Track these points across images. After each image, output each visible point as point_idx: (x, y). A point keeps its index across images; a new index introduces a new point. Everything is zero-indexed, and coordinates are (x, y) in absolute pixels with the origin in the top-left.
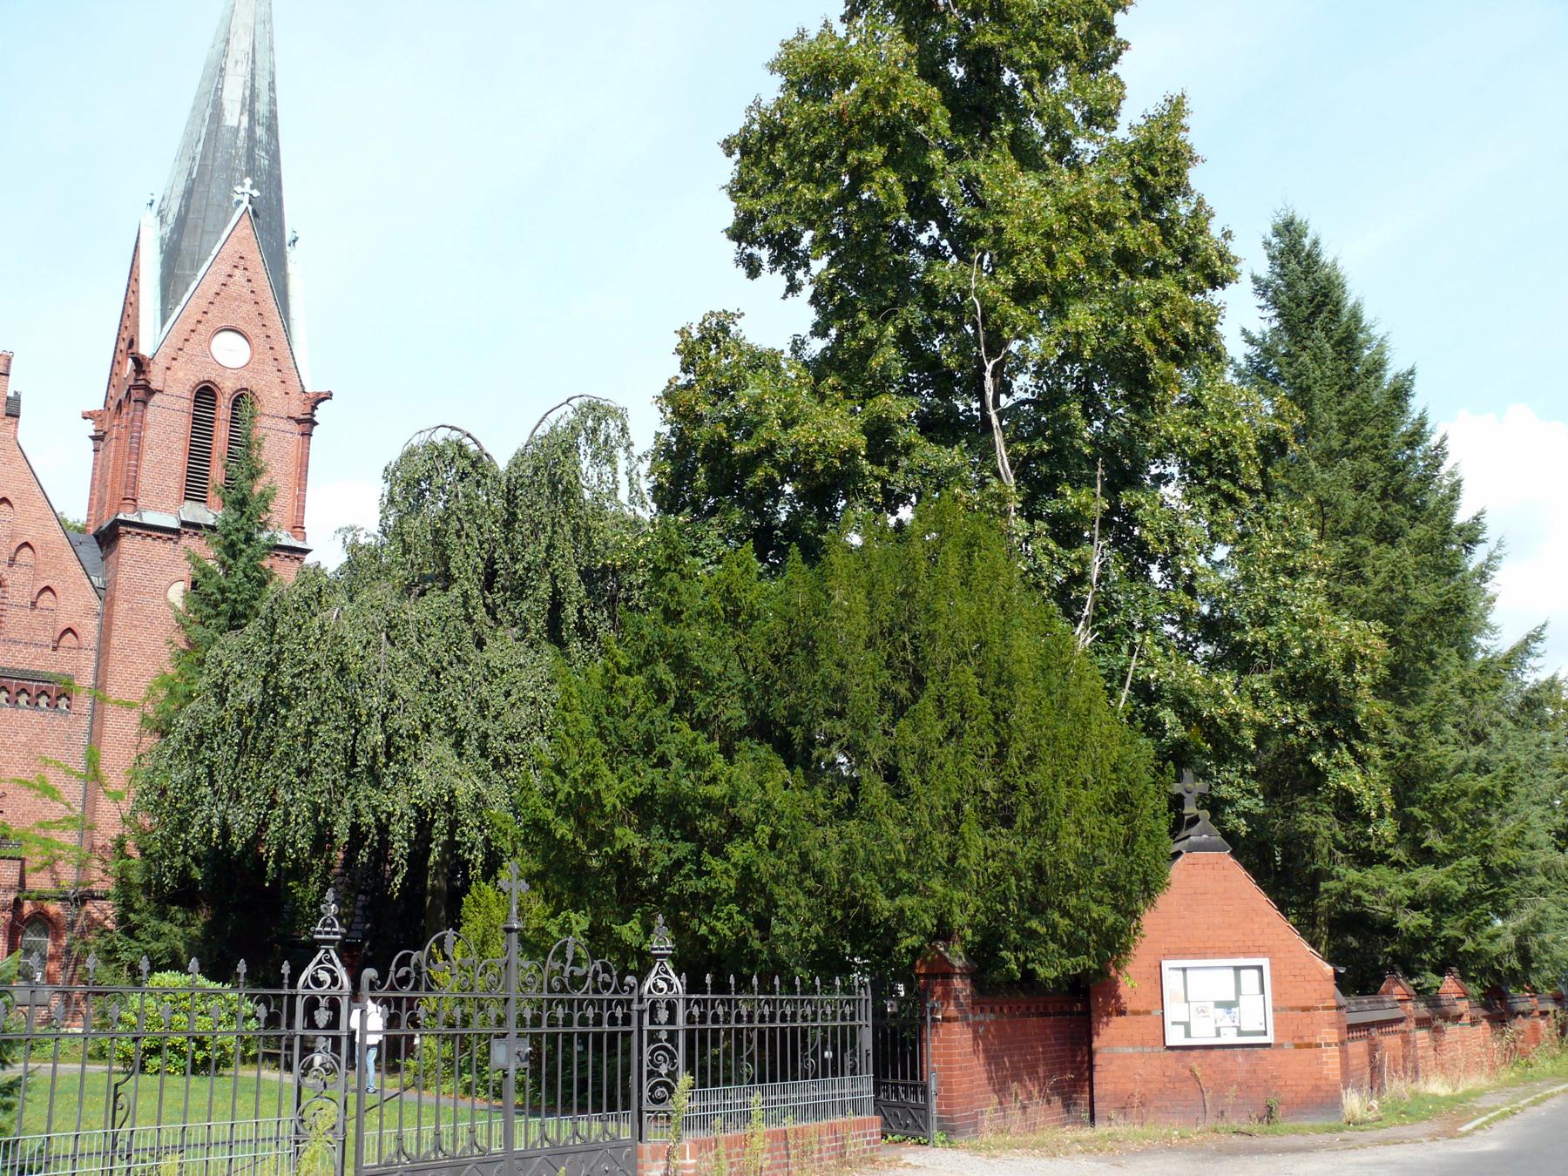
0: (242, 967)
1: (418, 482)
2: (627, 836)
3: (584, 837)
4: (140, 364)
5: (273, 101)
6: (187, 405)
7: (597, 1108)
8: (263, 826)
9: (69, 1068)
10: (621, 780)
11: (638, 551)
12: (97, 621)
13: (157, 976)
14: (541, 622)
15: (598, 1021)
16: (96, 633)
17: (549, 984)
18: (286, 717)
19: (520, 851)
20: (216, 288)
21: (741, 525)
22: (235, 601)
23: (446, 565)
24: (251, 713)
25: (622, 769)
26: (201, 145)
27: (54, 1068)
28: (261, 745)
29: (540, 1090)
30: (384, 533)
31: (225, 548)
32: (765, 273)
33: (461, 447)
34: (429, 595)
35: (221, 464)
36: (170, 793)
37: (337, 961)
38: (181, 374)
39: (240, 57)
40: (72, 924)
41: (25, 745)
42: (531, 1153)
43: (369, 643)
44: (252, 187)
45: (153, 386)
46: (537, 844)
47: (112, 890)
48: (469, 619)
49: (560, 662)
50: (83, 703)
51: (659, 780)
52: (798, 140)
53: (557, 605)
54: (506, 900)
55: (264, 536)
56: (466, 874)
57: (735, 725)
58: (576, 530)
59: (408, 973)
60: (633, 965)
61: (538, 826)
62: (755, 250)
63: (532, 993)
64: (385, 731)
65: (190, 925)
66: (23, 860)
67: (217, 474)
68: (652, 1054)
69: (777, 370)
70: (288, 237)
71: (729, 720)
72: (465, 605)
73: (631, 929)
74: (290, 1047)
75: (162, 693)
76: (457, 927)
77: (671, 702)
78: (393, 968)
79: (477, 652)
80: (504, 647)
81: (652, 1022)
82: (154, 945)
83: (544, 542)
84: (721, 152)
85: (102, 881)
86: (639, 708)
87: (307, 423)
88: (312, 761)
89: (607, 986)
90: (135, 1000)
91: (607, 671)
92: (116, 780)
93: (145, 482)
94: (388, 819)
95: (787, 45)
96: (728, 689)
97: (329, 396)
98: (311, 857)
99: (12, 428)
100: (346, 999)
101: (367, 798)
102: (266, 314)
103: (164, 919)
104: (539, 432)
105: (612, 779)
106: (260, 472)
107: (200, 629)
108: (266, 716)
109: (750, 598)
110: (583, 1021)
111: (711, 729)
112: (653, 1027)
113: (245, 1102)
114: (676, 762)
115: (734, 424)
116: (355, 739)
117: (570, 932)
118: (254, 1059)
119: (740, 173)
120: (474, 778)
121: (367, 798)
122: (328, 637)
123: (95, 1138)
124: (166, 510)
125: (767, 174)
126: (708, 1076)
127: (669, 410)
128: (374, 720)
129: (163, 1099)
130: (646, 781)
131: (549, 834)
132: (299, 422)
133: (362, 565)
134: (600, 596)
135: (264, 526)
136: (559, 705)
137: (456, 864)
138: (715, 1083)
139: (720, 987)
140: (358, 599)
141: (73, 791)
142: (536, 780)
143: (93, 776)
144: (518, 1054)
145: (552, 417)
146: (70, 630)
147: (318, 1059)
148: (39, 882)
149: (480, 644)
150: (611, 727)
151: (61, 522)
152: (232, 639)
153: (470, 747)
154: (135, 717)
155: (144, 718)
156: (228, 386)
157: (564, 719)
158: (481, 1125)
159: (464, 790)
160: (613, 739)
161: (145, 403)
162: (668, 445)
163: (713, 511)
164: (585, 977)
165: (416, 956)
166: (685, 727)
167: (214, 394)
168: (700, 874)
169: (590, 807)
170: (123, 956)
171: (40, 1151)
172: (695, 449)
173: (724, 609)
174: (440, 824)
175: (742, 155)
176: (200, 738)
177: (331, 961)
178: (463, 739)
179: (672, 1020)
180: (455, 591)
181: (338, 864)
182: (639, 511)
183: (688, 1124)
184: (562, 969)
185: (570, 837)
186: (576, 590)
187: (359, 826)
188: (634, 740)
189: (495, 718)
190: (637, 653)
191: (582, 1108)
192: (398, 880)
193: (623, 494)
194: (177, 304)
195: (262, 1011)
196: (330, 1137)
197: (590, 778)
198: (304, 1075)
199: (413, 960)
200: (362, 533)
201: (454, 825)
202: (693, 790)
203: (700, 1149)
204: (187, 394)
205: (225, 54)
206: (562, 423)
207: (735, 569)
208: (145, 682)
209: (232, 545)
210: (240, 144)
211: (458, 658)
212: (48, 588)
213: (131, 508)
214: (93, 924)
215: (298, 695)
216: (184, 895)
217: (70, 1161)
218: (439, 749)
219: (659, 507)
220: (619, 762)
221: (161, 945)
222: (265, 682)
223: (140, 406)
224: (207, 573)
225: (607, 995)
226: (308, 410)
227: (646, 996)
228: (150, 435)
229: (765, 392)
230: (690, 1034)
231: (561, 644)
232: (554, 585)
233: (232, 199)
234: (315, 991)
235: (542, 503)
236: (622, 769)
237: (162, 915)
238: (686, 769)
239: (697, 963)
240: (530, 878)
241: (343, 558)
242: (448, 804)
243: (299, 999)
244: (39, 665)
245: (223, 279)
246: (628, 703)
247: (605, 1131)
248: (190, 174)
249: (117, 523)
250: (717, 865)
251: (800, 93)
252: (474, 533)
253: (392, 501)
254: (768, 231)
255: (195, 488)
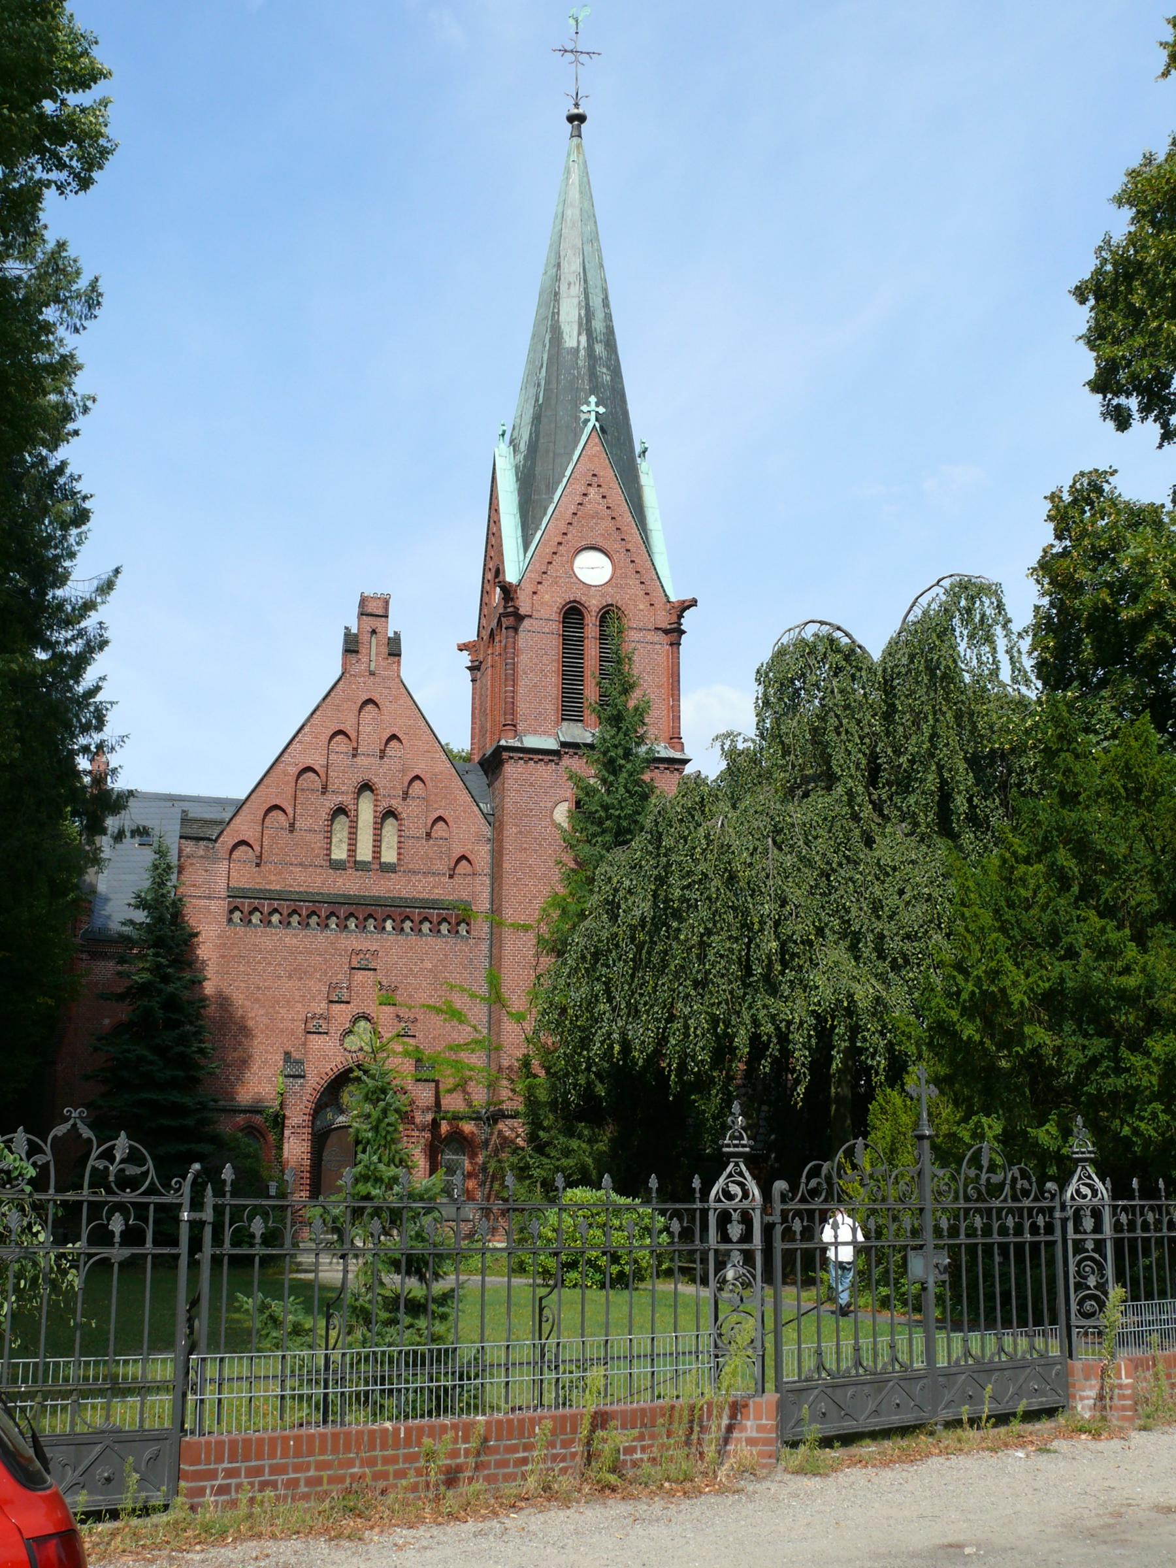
0: (653, 1182)
1: (792, 681)
2: (1038, 1035)
3: (992, 1036)
4: (508, 592)
5: (608, 317)
6: (556, 627)
7: (1023, 1323)
8: (662, 1040)
9: (496, 1281)
10: (1027, 975)
11: (1027, 732)
12: (488, 847)
13: (570, 1192)
14: (931, 816)
15: (1019, 1230)
16: (488, 859)
17: (965, 1192)
18: (679, 930)
19: (925, 1055)
20: (573, 508)
21: (1135, 696)
22: (619, 817)
23: (828, 763)
24: (643, 928)
25: (1027, 963)
26: (544, 370)
27: (483, 1281)
28: (655, 959)
29: (960, 1302)
30: (762, 736)
31: (604, 765)
32: (1136, 423)
33: (832, 641)
34: (813, 796)
35: (594, 682)
36: (570, 1011)
37: (747, 1174)
38: (547, 597)
39: (572, 279)
40: (486, 1143)
41: (431, 971)
42: (954, 1370)
43: (755, 849)
44: (597, 405)
45: (522, 611)
46: (943, 1047)
47: (521, 1108)
48: (855, 817)
49: (954, 856)
50: (482, 928)
51: (1068, 972)
52: (1157, 274)
53: (945, 796)
54: (917, 1104)
55: (643, 749)
56: (869, 1081)
57: (1146, 910)
58: (958, 716)
59: (819, 1184)
60: (1052, 1171)
61: (942, 1028)
62: (1122, 400)
63: (948, 1202)
64: (778, 938)
65: (597, 1142)
66: (437, 1082)
67: (591, 692)
68: (1078, 1265)
69: (1158, 525)
70: (638, 449)
71: (1139, 904)
72: (850, 803)
73: (1047, 1132)
74: (704, 1261)
75: (556, 914)
76: (865, 1135)
77: (1075, 889)
78: (803, 1180)
79: (866, 851)
80: (893, 846)
81: (1077, 1231)
82: (565, 1162)
83: (926, 730)
84: (1073, 301)
85: (511, 1099)
86: (1041, 898)
87: (675, 633)
88: (708, 972)
89: (1026, 1193)
90: (552, 1215)
91: (1004, 861)
92: (517, 1000)
93: (522, 707)
94: (788, 1027)
95: (1133, 174)
96: (1136, 871)
97: (694, 603)
98: (711, 1069)
99: (395, 667)
100: (758, 1212)
101: (765, 1006)
102: (624, 528)
103: (572, 1136)
104: (911, 618)
105: (1016, 974)
106: (632, 686)
107: (587, 847)
108: (658, 930)
109: (1152, 773)
110: (1003, 1231)
111: (1120, 915)
112: (1078, 1237)
113: (664, 1316)
114: (1085, 954)
115: (1117, 588)
116: (749, 948)
117: (982, 1137)
118: (669, 1273)
119: (1096, 320)
120: (873, 981)
121: (765, 1006)
122: (715, 846)
123: (524, 1350)
124: (545, 733)
125: (1126, 317)
126: (1140, 1290)
127: (1047, 580)
128: (767, 927)
129: (582, 1310)
130: (1054, 975)
131: (955, 1035)
132: (666, 632)
133: (742, 768)
134: (990, 784)
135: (641, 740)
136: (957, 900)
137: (857, 1069)
138: (1150, 1296)
139: (1149, 1192)
140: (742, 806)
141: (478, 1013)
142: (937, 980)
143: (496, 999)
144: (937, 1266)
145: (923, 601)
146: (463, 857)
147: (730, 1274)
148: (453, 1103)
149: (869, 842)
150: (1013, 920)
151: (447, 752)
152: (619, 855)
153: (867, 951)
154: (530, 939)
155: (540, 940)
156: (594, 604)
157: (963, 915)
158: (901, 1340)
159: (864, 994)
160: (1015, 932)
161: (516, 630)
162: (1049, 617)
163: (1103, 683)
164: (1003, 1184)
165: (826, 1166)
166: (1092, 914)
167: (581, 613)
168: (1118, 1071)
169: (995, 1005)
170: (535, 1173)
171: (476, 1359)
172: (1079, 619)
173: (1124, 787)
174: (840, 1030)
175: (1097, 299)
176: (596, 955)
177: (741, 1174)
178: (859, 941)
179: (1098, 1228)
180: (839, 790)
181: (739, 1075)
182: (1023, 689)
183: (1122, 1340)
184: (978, 1176)
185: (977, 1038)
186: (965, 779)
187: (760, 1036)
188: (1038, 931)
189: (891, 918)
190: (1034, 841)
191: (1007, 1323)
192: (801, 1089)
193: (1005, 675)
194: (537, 529)
195: (676, 1226)
196: (750, 1352)
197: (994, 974)
198: (721, 1289)
199: (824, 1171)
200: (740, 739)
201: (855, 1030)
202: (1105, 982)
203: (1136, 1368)
204: (555, 616)
205: (557, 279)
206: (934, 606)
207: (1133, 743)
208: (538, 904)
209: (612, 761)
210: (581, 363)
211: (847, 858)
212: (440, 818)
213: (511, 734)
214: (505, 1142)
215: (689, 907)
216: (583, 1113)
217: (503, 1369)
218: (835, 953)
219: (1045, 684)
220: (1023, 956)
221: (571, 1162)
222: (655, 895)
223: (511, 633)
224: (589, 792)
225: (1027, 1203)
226: (675, 619)
227: (1069, 1203)
228: (524, 660)
229: (1148, 550)
230: (1118, 1244)
231: (954, 836)
232: (941, 776)
233: (578, 421)
234: (727, 1204)
235: (921, 692)
236: (1027, 963)
237: (570, 1133)
238: (1096, 960)
239: (1116, 1166)
240: (937, 1081)
241: (723, 765)
242: (847, 1009)
243: (711, 1213)
244: (438, 893)
245: (578, 499)
246: (1029, 894)
247: (1032, 1347)
248: (537, 400)
249: (500, 749)
250: (1137, 1061)
251: (1153, 223)
252: (853, 728)
253: (767, 703)
254: (1134, 377)
255: (570, 709)
